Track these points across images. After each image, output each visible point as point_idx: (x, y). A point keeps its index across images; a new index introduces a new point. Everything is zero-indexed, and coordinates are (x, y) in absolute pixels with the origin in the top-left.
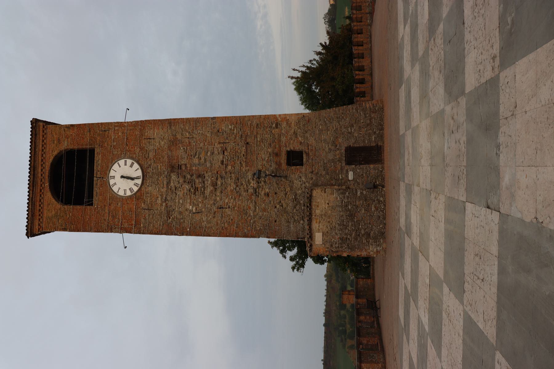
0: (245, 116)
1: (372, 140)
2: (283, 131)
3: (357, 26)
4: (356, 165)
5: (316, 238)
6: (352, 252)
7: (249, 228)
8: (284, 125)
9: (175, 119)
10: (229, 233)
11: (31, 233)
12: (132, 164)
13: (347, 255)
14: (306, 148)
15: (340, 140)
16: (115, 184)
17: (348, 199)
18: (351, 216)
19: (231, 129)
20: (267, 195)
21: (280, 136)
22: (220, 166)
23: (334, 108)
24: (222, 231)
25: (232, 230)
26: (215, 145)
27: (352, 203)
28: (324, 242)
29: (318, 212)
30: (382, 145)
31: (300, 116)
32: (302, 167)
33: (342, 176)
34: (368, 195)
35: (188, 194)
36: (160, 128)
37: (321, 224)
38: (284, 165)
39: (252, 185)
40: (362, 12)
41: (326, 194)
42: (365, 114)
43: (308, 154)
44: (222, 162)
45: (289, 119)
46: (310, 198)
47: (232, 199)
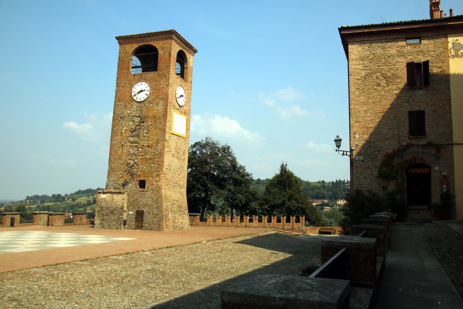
2: (154, 178)
3: (283, 219)
7: (113, 161)
8: (157, 179)
11: (117, 38)
12: (133, 92)
15: (147, 208)
16: (138, 86)
17: (119, 211)
18: (112, 212)
19: (158, 150)
21: (153, 176)
28: (102, 199)
31: (161, 187)
36: (163, 109)
38: (138, 179)
39: (132, 162)
40: (295, 223)
41: (121, 200)
42: (158, 221)
44: (143, 146)
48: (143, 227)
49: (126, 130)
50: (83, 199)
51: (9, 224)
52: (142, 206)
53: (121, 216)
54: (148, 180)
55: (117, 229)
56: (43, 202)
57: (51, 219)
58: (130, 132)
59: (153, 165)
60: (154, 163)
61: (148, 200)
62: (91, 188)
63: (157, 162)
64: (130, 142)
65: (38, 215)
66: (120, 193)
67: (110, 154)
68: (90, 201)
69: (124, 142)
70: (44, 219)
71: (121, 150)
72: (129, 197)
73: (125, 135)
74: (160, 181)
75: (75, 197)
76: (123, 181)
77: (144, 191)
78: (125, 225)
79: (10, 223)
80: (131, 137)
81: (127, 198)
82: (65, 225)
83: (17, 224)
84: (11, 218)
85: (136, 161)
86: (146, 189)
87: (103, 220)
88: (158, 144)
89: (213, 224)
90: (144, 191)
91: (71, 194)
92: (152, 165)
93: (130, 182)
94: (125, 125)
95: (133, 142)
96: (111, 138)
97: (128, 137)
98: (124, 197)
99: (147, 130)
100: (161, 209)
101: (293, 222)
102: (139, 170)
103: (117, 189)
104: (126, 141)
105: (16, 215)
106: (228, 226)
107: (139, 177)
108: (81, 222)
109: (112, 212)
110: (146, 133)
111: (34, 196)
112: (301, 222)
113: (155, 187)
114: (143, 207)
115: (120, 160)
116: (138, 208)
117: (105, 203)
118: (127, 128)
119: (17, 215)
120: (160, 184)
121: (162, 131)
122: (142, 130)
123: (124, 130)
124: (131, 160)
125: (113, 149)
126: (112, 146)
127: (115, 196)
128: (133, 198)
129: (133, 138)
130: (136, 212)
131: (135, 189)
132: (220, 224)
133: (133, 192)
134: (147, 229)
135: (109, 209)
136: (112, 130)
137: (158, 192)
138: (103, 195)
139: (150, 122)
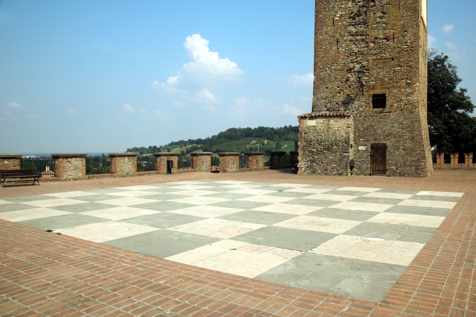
1: (391, 166)
7: (322, 67)
8: (409, 90)
14: (388, 111)
15: (393, 140)
17: (341, 146)
21: (399, 87)
25: (320, 53)
26: (392, 29)
30: (386, 174)
33: (362, 141)
37: (322, 124)
38: (372, 92)
39: (357, 65)
41: (345, 128)
42: (415, 161)
44: (376, 38)
45: (414, 94)
48: (386, 170)
49: (341, 16)
50: (176, 150)
51: (165, 170)
52: (382, 137)
53: (346, 154)
54: (391, 94)
55: (341, 175)
56: (142, 153)
57: (223, 162)
58: (350, 17)
59: (399, 68)
60: (399, 66)
61: (393, 127)
62: (183, 140)
63: (406, 62)
64: (350, 34)
65: (199, 157)
66: (342, 116)
67: (315, 56)
68: (184, 151)
69: (340, 36)
70: (206, 162)
71: (334, 48)
72: (357, 122)
73: (340, 23)
74: (415, 93)
75: (170, 148)
76: (344, 97)
77: (384, 111)
78: (352, 168)
79: (166, 169)
80: (352, 26)
81: (353, 124)
82: (240, 171)
83: (175, 171)
84: (168, 160)
85: (365, 63)
86: (387, 109)
87: (312, 162)
88: (406, 33)
89: (446, 166)
90: (384, 111)
91: (165, 145)
92: (396, 68)
93: (357, 99)
94: (340, 8)
95: (357, 34)
96: (315, 30)
97: (346, 27)
98: (350, 122)
99: (382, 12)
100: (419, 140)
102: (372, 78)
103: (334, 110)
104: (342, 33)
105: (173, 157)
106: (469, 169)
107: (373, 89)
108: (257, 166)
110: (381, 18)
111: (134, 148)
113: (405, 104)
114: (384, 138)
115: (334, 63)
116: (375, 139)
117: (315, 135)
118: (344, 13)
119: (175, 157)
120: (415, 100)
122: (372, 13)
123: (339, 15)
124: (355, 64)
125: (321, 48)
126: (318, 44)
127: (332, 121)
128: (364, 124)
129: (355, 28)
130: (372, 147)
131: (367, 109)
132: (456, 167)
133: (364, 114)
134: (394, 174)
135: (322, 143)
136: (315, 18)
138: (311, 121)
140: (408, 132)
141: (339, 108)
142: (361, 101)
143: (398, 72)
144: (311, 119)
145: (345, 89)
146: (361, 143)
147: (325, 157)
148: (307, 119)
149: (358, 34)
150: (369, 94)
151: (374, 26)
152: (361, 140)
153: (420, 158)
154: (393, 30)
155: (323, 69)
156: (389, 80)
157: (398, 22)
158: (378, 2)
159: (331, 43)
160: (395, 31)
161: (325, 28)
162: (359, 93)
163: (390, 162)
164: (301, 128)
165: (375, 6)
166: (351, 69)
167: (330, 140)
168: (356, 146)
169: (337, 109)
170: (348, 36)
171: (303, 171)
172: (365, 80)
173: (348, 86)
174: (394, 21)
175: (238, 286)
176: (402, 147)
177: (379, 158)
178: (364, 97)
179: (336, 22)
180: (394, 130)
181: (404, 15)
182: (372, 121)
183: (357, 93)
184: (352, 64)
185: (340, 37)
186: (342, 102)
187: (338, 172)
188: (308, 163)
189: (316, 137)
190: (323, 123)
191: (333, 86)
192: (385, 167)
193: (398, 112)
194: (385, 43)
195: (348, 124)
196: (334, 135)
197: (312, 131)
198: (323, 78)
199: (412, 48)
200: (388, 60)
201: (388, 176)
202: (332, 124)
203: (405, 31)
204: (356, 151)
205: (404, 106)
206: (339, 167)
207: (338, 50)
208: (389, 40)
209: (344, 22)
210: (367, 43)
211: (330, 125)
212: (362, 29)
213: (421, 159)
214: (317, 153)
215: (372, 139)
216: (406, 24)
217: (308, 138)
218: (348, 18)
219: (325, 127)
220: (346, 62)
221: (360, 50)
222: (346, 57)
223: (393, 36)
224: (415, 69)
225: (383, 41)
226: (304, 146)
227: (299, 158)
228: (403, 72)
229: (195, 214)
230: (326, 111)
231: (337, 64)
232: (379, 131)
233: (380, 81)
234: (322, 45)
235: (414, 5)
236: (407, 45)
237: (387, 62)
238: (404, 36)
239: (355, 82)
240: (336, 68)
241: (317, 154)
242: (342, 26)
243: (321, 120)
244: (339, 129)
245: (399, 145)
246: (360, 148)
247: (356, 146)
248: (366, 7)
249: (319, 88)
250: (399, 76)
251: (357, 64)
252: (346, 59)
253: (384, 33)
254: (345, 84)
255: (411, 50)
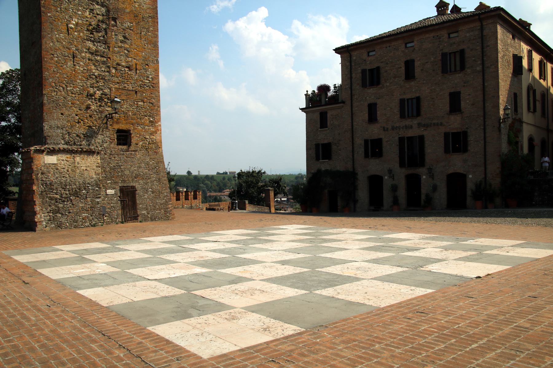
0: (159, 93)
1: (142, 211)
2: (146, 127)
4: (120, 197)
5: (51, 157)
6: (38, 195)
7: (54, 84)
9: (158, 24)
10: (47, 61)
13: (34, 190)
14: (133, 149)
15: (141, 182)
17: (92, 190)
18: (76, 194)
19: (148, 77)
20: (88, 108)
21: (143, 124)
22: (115, 61)
23: (166, 176)
24: (49, 54)
25: (51, 65)
26: (134, 59)
27: (88, 194)
29: (78, 159)
30: (139, 220)
31: (159, 144)
32: (116, 144)
33: (109, 183)
34: (97, 209)
35: (87, 23)
36: (150, 6)
37: (65, 162)
38: (116, 127)
39: (98, 92)
41: (95, 167)
43: (127, 151)
44: (118, 64)
45: (157, 133)
46: (90, 152)
47: (83, 69)
52: (130, 179)
54: (136, 131)
55: (94, 226)
58: (88, 30)
59: (142, 103)
61: (140, 167)
63: (148, 98)
69: (77, 50)
73: (76, 33)
80: (91, 41)
85: (107, 91)
86: (132, 148)
87: (57, 211)
93: (100, 133)
95: (95, 53)
101: (191, 199)
104: (80, 46)
107: (117, 123)
109: (76, 194)
110: (122, 42)
112: (198, 198)
114: (133, 180)
117: (57, 176)
121: (152, 45)
124: (96, 89)
128: (110, 163)
129: (94, 45)
130: (122, 190)
131: (112, 145)
133: (109, 152)
134: (146, 219)
135: (68, 187)
137: (155, 152)
139: (129, 24)
140: (155, 173)
141: (81, 142)
142: (105, 135)
143: (141, 107)
144: (49, 154)
145: (85, 118)
146: (109, 185)
147: (73, 204)
148: (44, 154)
149: (99, 54)
150: (114, 129)
151: (115, 49)
152: (108, 182)
153: (168, 200)
154: (135, 60)
155: (56, 88)
156: (133, 115)
157: (140, 53)
158: (120, 23)
159: (65, 56)
160: (137, 62)
161: (56, 33)
162: (102, 126)
163: (141, 206)
164: (35, 166)
165: (117, 26)
166: (92, 95)
167: (77, 183)
168: (104, 190)
169: (79, 143)
170: (86, 52)
171: (45, 226)
172: (108, 111)
173: (88, 115)
174: (135, 50)
175: (386, 345)
176: (151, 190)
177: (130, 202)
178: (108, 131)
179: (71, 30)
180: (142, 171)
181: (146, 47)
182: (118, 160)
183: (100, 125)
184: (92, 89)
185: (77, 52)
186: (83, 134)
187: (90, 222)
188: (50, 214)
189: (59, 178)
190: (66, 160)
191: (70, 113)
192: (137, 212)
193: (143, 151)
194: (128, 73)
195: (98, 163)
196: (82, 176)
197: (52, 171)
198: (57, 100)
199: (153, 84)
200: (131, 93)
201: (140, 222)
202: (78, 162)
203: (146, 65)
204: (104, 195)
205: (148, 145)
206: (91, 216)
207: (75, 67)
208: (132, 70)
209: (81, 34)
210: (109, 67)
211: (76, 164)
212: (102, 49)
213: (168, 201)
214: (61, 200)
215: (120, 181)
216: (147, 57)
217: (48, 179)
218: (86, 31)
219: (70, 166)
220: (85, 85)
221: (101, 73)
222: (84, 79)
223: (135, 67)
224: (157, 108)
225: (125, 70)
226: (42, 192)
227: (37, 208)
228: (146, 109)
229: (347, 273)
230: (64, 144)
231: (73, 85)
232: (127, 172)
233: (124, 114)
234: (53, 55)
235: (154, 39)
236: (149, 80)
237: (131, 94)
238: (146, 70)
239: (96, 112)
240: (73, 90)
241: (62, 201)
242: (78, 37)
243: (64, 157)
244: (88, 169)
245: (148, 187)
246: (108, 192)
247: (104, 190)
248: (106, 24)
249: (51, 113)
250: (142, 112)
251: (98, 90)
252: (85, 81)
253: (126, 61)
254: (85, 112)
255: (152, 86)
